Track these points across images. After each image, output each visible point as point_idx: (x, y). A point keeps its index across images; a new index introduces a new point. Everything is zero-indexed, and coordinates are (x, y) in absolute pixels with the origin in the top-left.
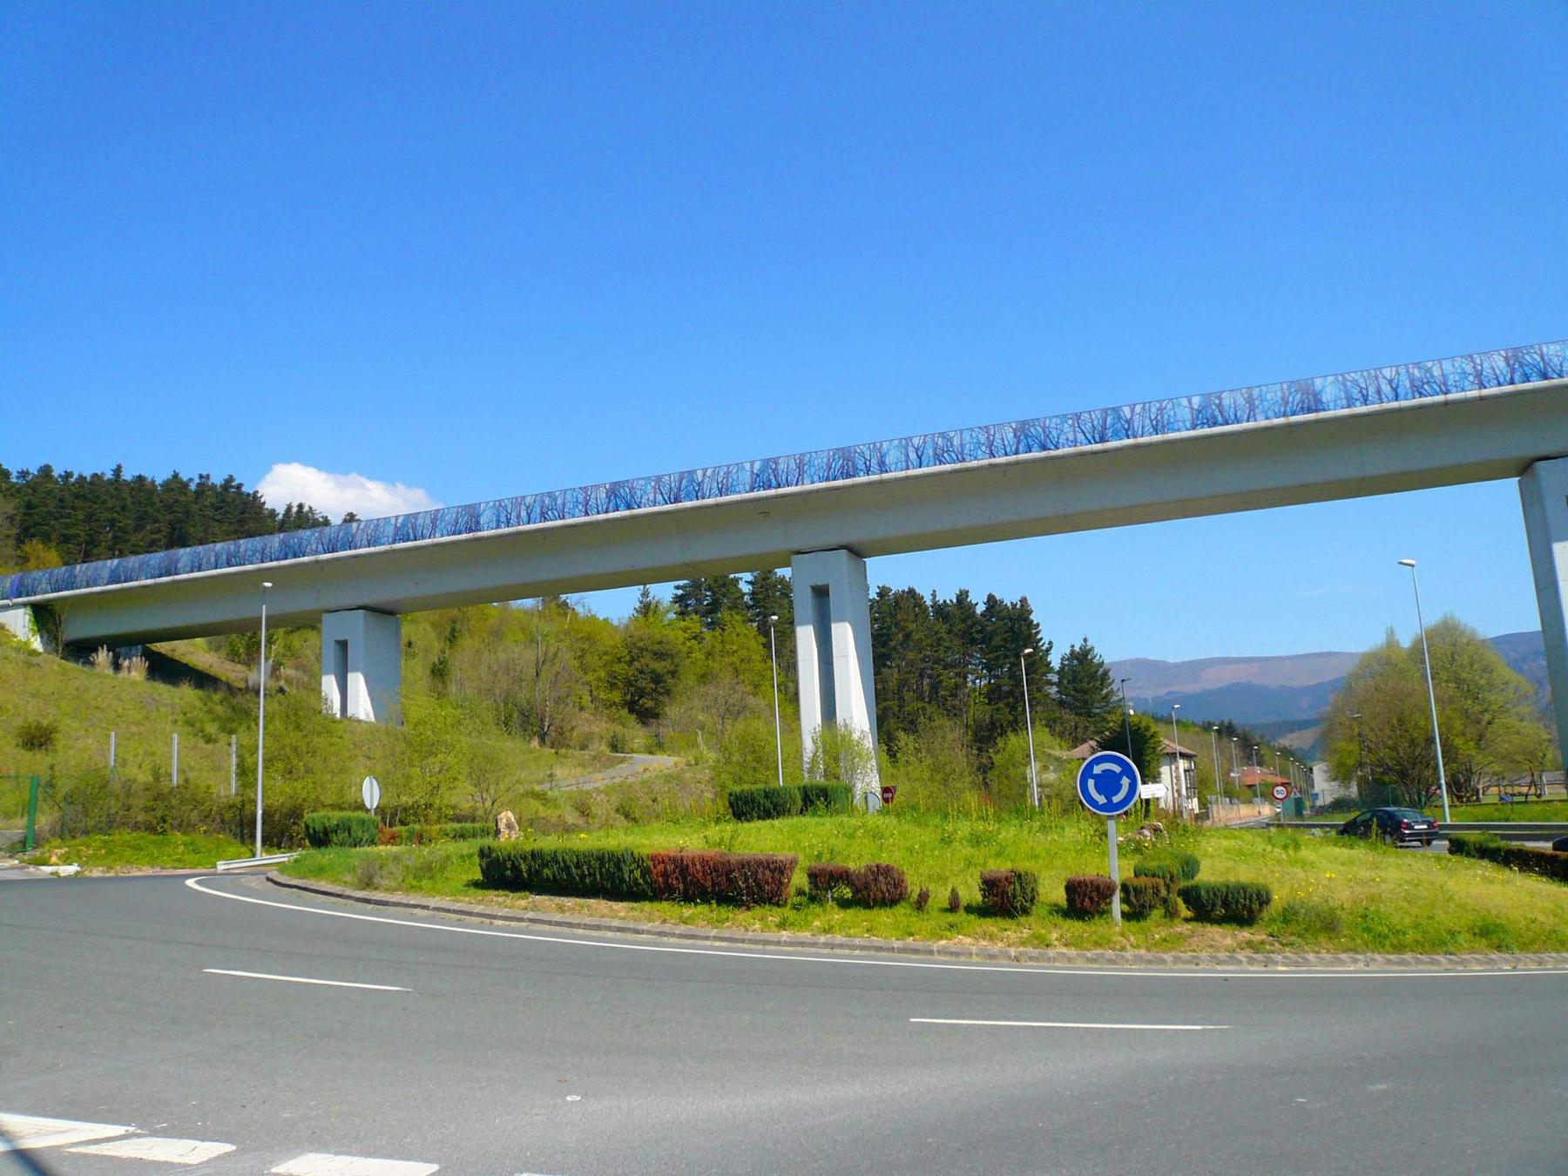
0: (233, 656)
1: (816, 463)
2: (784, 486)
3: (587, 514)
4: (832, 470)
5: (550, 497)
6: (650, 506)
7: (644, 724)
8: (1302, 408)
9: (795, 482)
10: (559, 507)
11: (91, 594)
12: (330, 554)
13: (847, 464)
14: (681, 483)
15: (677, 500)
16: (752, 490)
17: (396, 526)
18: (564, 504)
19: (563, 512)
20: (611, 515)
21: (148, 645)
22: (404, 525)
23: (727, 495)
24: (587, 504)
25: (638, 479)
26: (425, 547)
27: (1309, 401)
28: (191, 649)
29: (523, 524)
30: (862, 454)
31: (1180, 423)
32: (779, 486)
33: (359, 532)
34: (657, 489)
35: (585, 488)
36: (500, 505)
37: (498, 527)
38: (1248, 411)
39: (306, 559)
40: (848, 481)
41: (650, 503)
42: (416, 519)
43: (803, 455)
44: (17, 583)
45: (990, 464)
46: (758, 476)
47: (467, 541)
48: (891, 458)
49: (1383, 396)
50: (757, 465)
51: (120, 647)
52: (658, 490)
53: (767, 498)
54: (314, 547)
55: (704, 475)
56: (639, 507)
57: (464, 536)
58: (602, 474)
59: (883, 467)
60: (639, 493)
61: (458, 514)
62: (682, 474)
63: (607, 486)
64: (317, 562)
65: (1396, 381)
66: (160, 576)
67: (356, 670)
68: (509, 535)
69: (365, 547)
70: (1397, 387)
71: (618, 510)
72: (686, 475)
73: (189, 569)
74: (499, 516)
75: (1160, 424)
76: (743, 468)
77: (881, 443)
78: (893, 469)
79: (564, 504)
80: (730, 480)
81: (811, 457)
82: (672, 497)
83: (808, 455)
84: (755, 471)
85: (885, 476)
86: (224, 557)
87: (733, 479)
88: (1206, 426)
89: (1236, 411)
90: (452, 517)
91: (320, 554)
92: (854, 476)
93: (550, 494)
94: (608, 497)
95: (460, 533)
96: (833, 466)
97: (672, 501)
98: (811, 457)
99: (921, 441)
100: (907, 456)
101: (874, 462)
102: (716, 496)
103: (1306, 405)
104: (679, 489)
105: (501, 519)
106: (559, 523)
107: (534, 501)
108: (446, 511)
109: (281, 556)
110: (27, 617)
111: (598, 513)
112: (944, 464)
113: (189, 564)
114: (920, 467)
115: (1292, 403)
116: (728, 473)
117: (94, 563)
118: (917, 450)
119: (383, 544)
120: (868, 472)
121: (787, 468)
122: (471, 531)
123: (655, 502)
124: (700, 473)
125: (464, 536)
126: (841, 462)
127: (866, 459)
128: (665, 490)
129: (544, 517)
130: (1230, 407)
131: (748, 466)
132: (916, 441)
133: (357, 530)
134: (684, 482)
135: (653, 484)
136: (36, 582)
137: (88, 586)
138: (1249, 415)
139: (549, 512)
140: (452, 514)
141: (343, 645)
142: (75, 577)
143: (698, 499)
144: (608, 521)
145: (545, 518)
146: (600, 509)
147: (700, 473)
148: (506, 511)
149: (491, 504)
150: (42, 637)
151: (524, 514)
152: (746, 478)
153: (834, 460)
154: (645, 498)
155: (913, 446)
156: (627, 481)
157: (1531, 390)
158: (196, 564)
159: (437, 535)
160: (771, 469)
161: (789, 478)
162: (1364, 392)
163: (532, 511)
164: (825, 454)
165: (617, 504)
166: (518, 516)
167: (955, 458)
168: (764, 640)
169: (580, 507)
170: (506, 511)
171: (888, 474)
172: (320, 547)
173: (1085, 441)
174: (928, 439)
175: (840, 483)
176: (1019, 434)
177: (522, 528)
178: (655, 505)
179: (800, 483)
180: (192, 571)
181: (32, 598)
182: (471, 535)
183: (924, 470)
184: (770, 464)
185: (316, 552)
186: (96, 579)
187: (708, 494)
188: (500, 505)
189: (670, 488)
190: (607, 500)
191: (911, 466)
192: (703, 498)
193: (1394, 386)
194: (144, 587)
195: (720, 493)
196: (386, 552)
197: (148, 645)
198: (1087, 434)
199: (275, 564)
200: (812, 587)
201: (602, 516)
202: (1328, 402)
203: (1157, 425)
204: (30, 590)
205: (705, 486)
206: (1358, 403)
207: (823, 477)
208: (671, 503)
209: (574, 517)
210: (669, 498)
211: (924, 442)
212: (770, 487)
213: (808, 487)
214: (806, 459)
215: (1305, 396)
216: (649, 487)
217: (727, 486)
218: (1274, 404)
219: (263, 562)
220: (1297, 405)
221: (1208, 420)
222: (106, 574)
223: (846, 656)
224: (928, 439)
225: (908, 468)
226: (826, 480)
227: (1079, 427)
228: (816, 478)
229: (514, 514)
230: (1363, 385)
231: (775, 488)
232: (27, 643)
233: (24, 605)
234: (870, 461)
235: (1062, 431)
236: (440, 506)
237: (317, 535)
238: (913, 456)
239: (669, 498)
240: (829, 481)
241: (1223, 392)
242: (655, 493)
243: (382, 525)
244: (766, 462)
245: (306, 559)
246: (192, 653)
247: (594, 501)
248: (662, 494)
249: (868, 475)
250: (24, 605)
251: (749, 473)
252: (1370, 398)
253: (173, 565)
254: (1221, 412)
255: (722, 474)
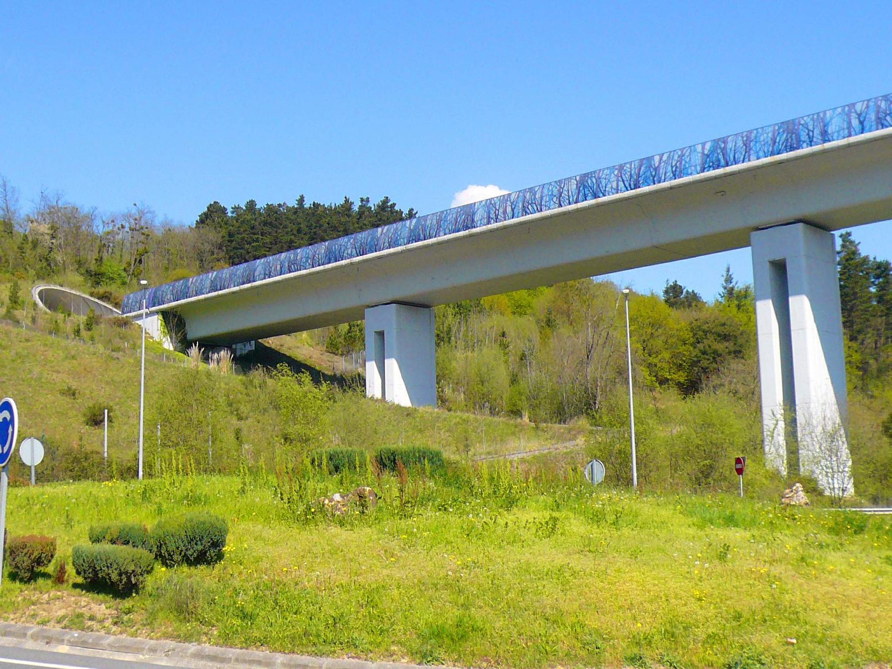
0: (333, 348)
1: (762, 138)
2: (732, 165)
3: (560, 206)
4: (777, 144)
5: (886, 101)
6: (613, 194)
7: (697, 390)
8: (786, 146)
9: (742, 159)
10: (538, 201)
11: (199, 301)
12: (633, 191)
13: (791, 137)
14: (640, 169)
15: (637, 186)
16: (703, 170)
17: (703, 153)
18: (542, 198)
19: (541, 205)
20: (580, 205)
21: (260, 340)
22: (713, 150)
23: (681, 177)
24: (561, 196)
25: (604, 170)
26: (432, 245)
27: (792, 140)
28: (299, 345)
29: (856, 134)
30: (806, 126)
31: (693, 168)
32: (727, 165)
33: (663, 164)
34: (620, 177)
35: (560, 181)
36: (491, 203)
37: (489, 223)
38: (744, 153)
39: (343, 262)
40: (792, 154)
41: (613, 191)
42: (725, 142)
43: (751, 132)
44: (152, 295)
45: (351, 263)
46: (708, 156)
47: (464, 237)
48: (834, 127)
49: (852, 130)
50: (708, 146)
51: (236, 343)
52: (620, 178)
53: (716, 178)
54: (349, 252)
55: (661, 159)
56: (604, 195)
57: (462, 233)
58: (574, 168)
59: (825, 136)
60: (603, 182)
61: (774, 133)
62: (641, 160)
63: (578, 178)
64: (352, 264)
65: (864, 115)
66: (243, 284)
67: (798, 293)
68: (498, 229)
69: (387, 248)
70: (864, 120)
71: (586, 200)
72: (645, 162)
73: (262, 276)
74: (489, 213)
75: (678, 169)
76: (695, 151)
77: (825, 112)
78: (835, 138)
79: (542, 198)
80: (683, 162)
81: (757, 132)
82: (632, 183)
83: (755, 132)
84: (706, 152)
85: (828, 145)
86: (873, 116)
87: (686, 162)
88: (711, 169)
89: (735, 153)
90: (767, 137)
91: (354, 257)
92: (797, 148)
93: (531, 190)
94: (578, 188)
95: (458, 231)
96: (777, 141)
97: (632, 186)
98: (757, 132)
99: (865, 106)
100: (850, 123)
101: (817, 132)
102: (671, 179)
103: (789, 144)
104: (639, 176)
105: (491, 216)
106: (537, 215)
107: (518, 197)
108: (448, 211)
109: (326, 261)
110: (160, 321)
111: (570, 203)
112: (887, 127)
113: (262, 272)
114: (862, 133)
115: (779, 143)
116: (681, 157)
117: (395, 225)
118: (859, 115)
119: (401, 245)
120: (811, 143)
121: (735, 146)
122: (467, 228)
123: (618, 190)
124: (657, 158)
125: (462, 233)
126: (785, 135)
127: (809, 130)
128: (626, 177)
129: (525, 212)
130: (731, 150)
131: (699, 148)
132: (859, 107)
133: (660, 163)
134: (643, 168)
135: (616, 172)
136: (165, 294)
137: (197, 295)
138: (745, 156)
139: (530, 207)
140: (767, 134)
141: (381, 334)
142: (378, 240)
143: (654, 184)
144: (578, 210)
145: (526, 212)
146: (571, 200)
147: (657, 158)
148: (807, 129)
149: (839, 110)
150: (171, 338)
151: (509, 209)
152: (697, 159)
153: (779, 134)
154: (609, 186)
155: (856, 112)
156: (595, 172)
157: (845, 145)
158: (267, 272)
159: (752, 157)
160: (720, 148)
161: (736, 156)
162: (811, 134)
163: (865, 118)
164: (771, 129)
165: (585, 194)
166: (505, 212)
167: (536, 209)
168: (111, 414)
169: (555, 199)
170: (807, 129)
171: (830, 143)
172: (621, 184)
173: (624, 189)
174: (871, 104)
175: (784, 156)
176: (579, 185)
177: (507, 223)
178: (617, 193)
179: (747, 160)
180: (265, 278)
181: (162, 307)
182: (466, 232)
183: (867, 135)
184: (720, 144)
185: (351, 256)
186: (202, 289)
187: (663, 178)
188: (491, 203)
189: (631, 175)
190: (577, 191)
191: (853, 133)
192: (659, 182)
193: (862, 119)
194: (233, 293)
195: (674, 175)
196: (402, 252)
197: (260, 340)
198: (626, 182)
199: (321, 268)
200: (770, 262)
201: (573, 207)
202: (833, 133)
203: (675, 171)
204: (338, 255)
205: (661, 171)
206: (805, 145)
207: (768, 151)
208: (631, 189)
209: (549, 208)
210: (630, 185)
211: (867, 107)
212: (718, 167)
213: (754, 163)
214: (753, 135)
215: (789, 135)
216: (613, 175)
217: (680, 168)
218: (764, 145)
219: (313, 267)
220: (782, 144)
221: (713, 163)
222: (208, 284)
223: (803, 329)
224: (871, 104)
225: (850, 135)
226: (771, 155)
227: (621, 176)
228: (761, 154)
229: (501, 210)
230: (811, 128)
231: (723, 167)
232: (160, 343)
233: (157, 312)
234: (813, 132)
235: (609, 181)
236: (506, 192)
237: (352, 241)
238: (855, 123)
239: (630, 185)
240: (774, 155)
241: (729, 137)
242: (618, 181)
243: (687, 154)
244: (716, 142)
245: (343, 262)
246: (298, 347)
247: (566, 193)
248: (623, 181)
249: (811, 146)
250: (157, 312)
251: (700, 155)
252: (815, 140)
253: (252, 273)
254: (723, 155)
255: (676, 157)
